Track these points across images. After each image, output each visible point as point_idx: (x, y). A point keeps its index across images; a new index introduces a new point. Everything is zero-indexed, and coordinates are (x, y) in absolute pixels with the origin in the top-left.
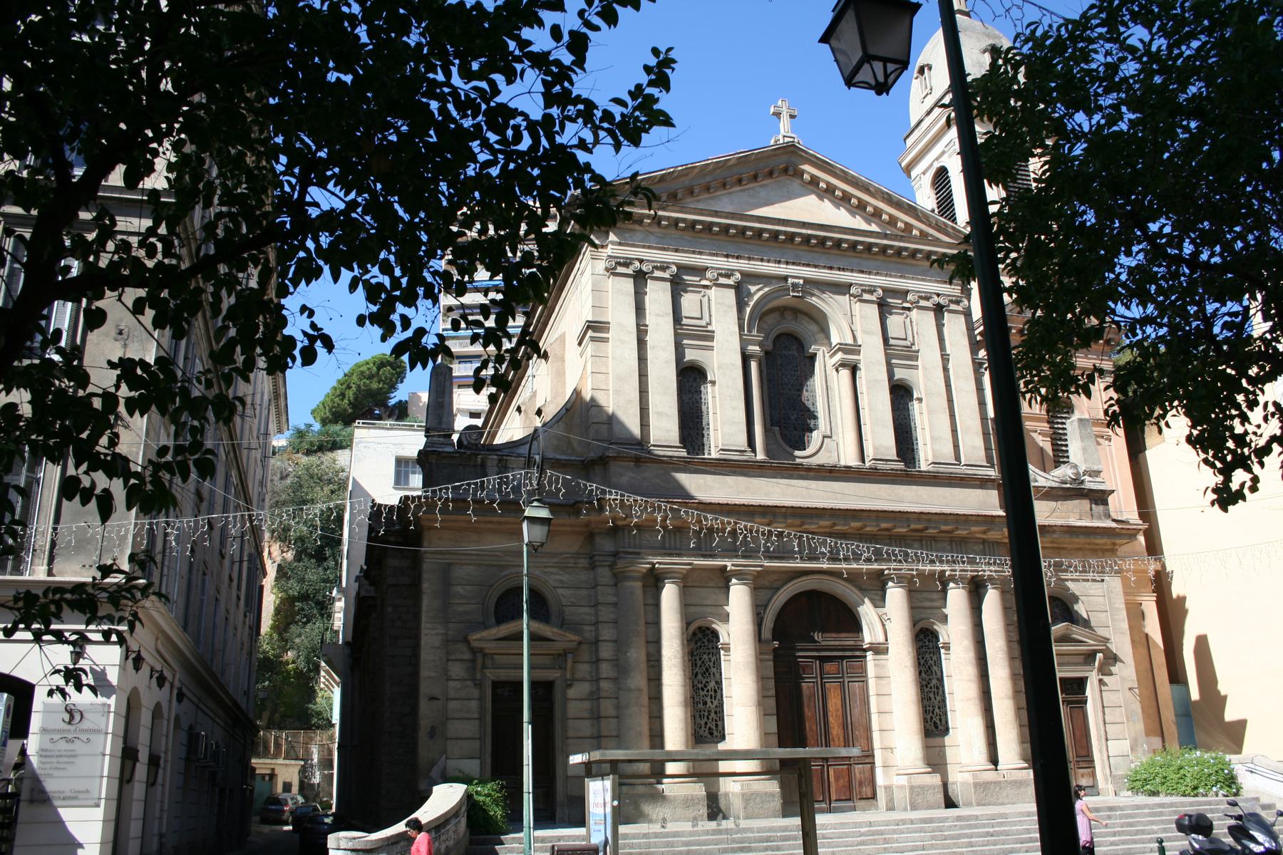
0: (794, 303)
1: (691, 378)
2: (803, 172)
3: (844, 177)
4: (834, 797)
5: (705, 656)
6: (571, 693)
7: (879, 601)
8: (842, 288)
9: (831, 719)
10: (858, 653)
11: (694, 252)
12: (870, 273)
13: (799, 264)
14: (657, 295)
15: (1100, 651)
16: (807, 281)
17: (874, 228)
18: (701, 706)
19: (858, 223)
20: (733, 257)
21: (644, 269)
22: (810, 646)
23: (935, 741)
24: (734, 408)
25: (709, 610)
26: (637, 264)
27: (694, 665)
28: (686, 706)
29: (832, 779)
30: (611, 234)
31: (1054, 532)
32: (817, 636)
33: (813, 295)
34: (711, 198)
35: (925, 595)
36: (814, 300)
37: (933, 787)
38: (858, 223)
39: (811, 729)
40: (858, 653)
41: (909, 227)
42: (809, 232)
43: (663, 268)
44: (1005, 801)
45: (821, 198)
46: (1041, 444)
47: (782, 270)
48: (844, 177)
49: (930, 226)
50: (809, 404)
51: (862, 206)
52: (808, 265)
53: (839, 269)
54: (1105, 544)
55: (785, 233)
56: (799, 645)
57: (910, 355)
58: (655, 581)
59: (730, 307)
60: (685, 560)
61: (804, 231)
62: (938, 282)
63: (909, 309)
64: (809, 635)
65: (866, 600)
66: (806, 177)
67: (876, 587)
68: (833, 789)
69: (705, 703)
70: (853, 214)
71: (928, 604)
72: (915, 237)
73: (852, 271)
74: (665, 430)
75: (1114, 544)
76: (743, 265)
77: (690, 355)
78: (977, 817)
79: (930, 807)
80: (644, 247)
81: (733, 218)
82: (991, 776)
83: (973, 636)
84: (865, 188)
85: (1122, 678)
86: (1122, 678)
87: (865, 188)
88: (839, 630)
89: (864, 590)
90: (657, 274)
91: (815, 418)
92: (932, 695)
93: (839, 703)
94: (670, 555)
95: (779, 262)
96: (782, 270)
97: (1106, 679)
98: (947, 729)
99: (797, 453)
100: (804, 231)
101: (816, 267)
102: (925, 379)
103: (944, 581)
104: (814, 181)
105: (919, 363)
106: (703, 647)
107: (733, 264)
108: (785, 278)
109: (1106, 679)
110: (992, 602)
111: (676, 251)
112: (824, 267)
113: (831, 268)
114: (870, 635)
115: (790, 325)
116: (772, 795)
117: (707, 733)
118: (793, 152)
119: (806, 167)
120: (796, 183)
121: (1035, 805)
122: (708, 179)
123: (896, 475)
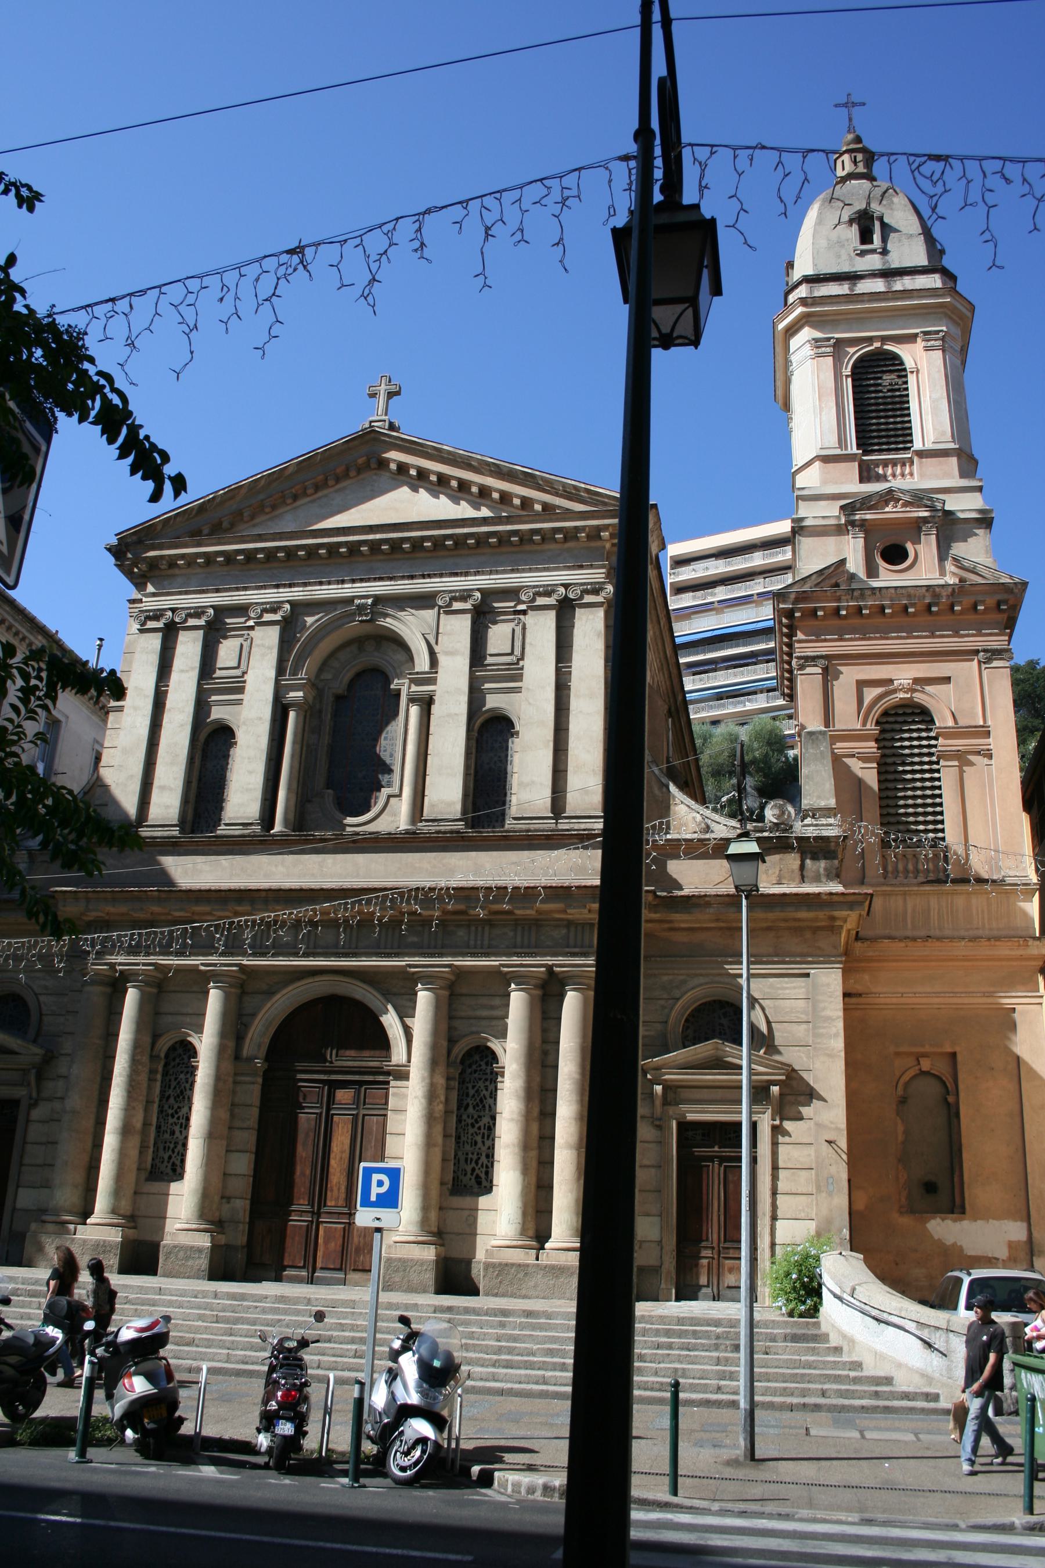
0: (368, 628)
1: (212, 744)
2: (388, 461)
3: (438, 455)
4: (319, 1265)
5: (182, 1076)
6: (35, 1114)
7: (405, 1012)
8: (424, 601)
9: (333, 1162)
10: (381, 1078)
11: (237, 589)
12: (467, 574)
13: (368, 580)
14: (188, 648)
15: (775, 1083)
16: (378, 600)
17: (485, 512)
18: (167, 1136)
19: (464, 510)
20: (284, 586)
21: (571, 596)
22: (317, 1066)
23: (458, 1201)
24: (250, 772)
25: (188, 1019)
26: (562, 590)
27: (463, 1095)
28: (578, 1148)
29: (321, 1241)
30: (149, 585)
31: (708, 904)
32: (330, 1054)
33: (386, 615)
34: (271, 519)
35: (484, 1001)
36: (389, 622)
37: (422, 1263)
38: (464, 510)
39: (303, 1174)
40: (381, 1078)
41: (526, 503)
42: (378, 536)
43: (198, 613)
44: (531, 1293)
45: (415, 489)
46: (860, 773)
47: (347, 590)
48: (438, 455)
49: (557, 495)
50: (385, 756)
51: (464, 486)
52: (381, 579)
53: (423, 576)
54: (816, 919)
55: (346, 544)
56: (300, 1065)
57: (513, 673)
58: (117, 985)
59: (270, 648)
60: (447, 960)
61: (371, 537)
62: (569, 568)
63: (251, 628)
64: (310, 1054)
65: (390, 1007)
66: (393, 466)
67: (400, 991)
68: (320, 1254)
69: (173, 1133)
70: (456, 500)
71: (485, 1013)
72: (537, 514)
73: (441, 575)
74: (167, 804)
75: (833, 918)
76: (297, 593)
77: (493, 702)
78: (549, 1315)
79: (411, 1289)
80: (180, 593)
81: (281, 540)
82: (527, 1257)
83: (541, 1056)
84: (465, 463)
85: (817, 1125)
86: (817, 1125)
87: (465, 463)
88: (361, 1047)
89: (389, 995)
90: (589, 599)
91: (389, 771)
92: (479, 1139)
93: (347, 1142)
94: (432, 955)
95: (343, 582)
96: (347, 590)
97: (788, 1125)
98: (491, 1188)
99: (350, 820)
100: (371, 537)
101: (391, 579)
102: (531, 707)
103: (501, 981)
104: (403, 468)
105: (245, 697)
106: (167, 1068)
107: (270, 595)
108: (350, 601)
109: (788, 1125)
110: (572, 1007)
111: (217, 591)
112: (403, 578)
113: (412, 577)
114: (398, 1054)
115: (372, 658)
116: (200, 1250)
117: (169, 1170)
118: (375, 439)
119: (393, 455)
120: (385, 476)
121: (574, 1303)
122: (261, 497)
123: (447, 839)
